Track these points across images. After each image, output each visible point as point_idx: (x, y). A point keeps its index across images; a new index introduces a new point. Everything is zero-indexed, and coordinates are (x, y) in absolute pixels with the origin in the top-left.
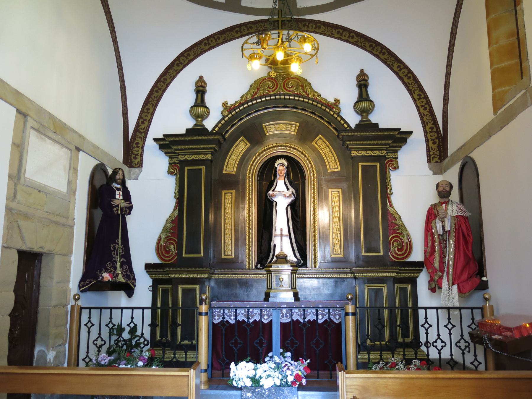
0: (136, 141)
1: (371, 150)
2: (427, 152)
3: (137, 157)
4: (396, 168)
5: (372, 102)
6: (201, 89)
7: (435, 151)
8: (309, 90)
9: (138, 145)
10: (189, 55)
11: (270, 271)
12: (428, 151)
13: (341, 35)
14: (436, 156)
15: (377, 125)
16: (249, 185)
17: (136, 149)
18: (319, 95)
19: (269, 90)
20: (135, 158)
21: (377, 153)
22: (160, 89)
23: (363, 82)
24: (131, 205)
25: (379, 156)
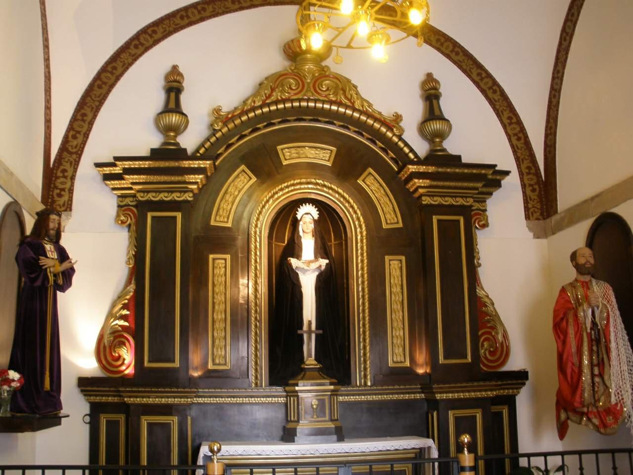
0: (62, 167)
1: (440, 196)
2: (524, 203)
3: (63, 193)
4: (485, 226)
5: (448, 121)
6: (174, 87)
7: (535, 204)
8: (355, 96)
9: (66, 174)
10: (155, 32)
11: (297, 392)
12: (526, 202)
13: (528, 174)
14: (536, 210)
15: (459, 158)
16: (256, 247)
17: (62, 180)
18: (370, 105)
19: (290, 91)
20: (60, 195)
21: (460, 201)
22: (105, 83)
23: (431, 94)
24: (66, 265)
25: (463, 206)
